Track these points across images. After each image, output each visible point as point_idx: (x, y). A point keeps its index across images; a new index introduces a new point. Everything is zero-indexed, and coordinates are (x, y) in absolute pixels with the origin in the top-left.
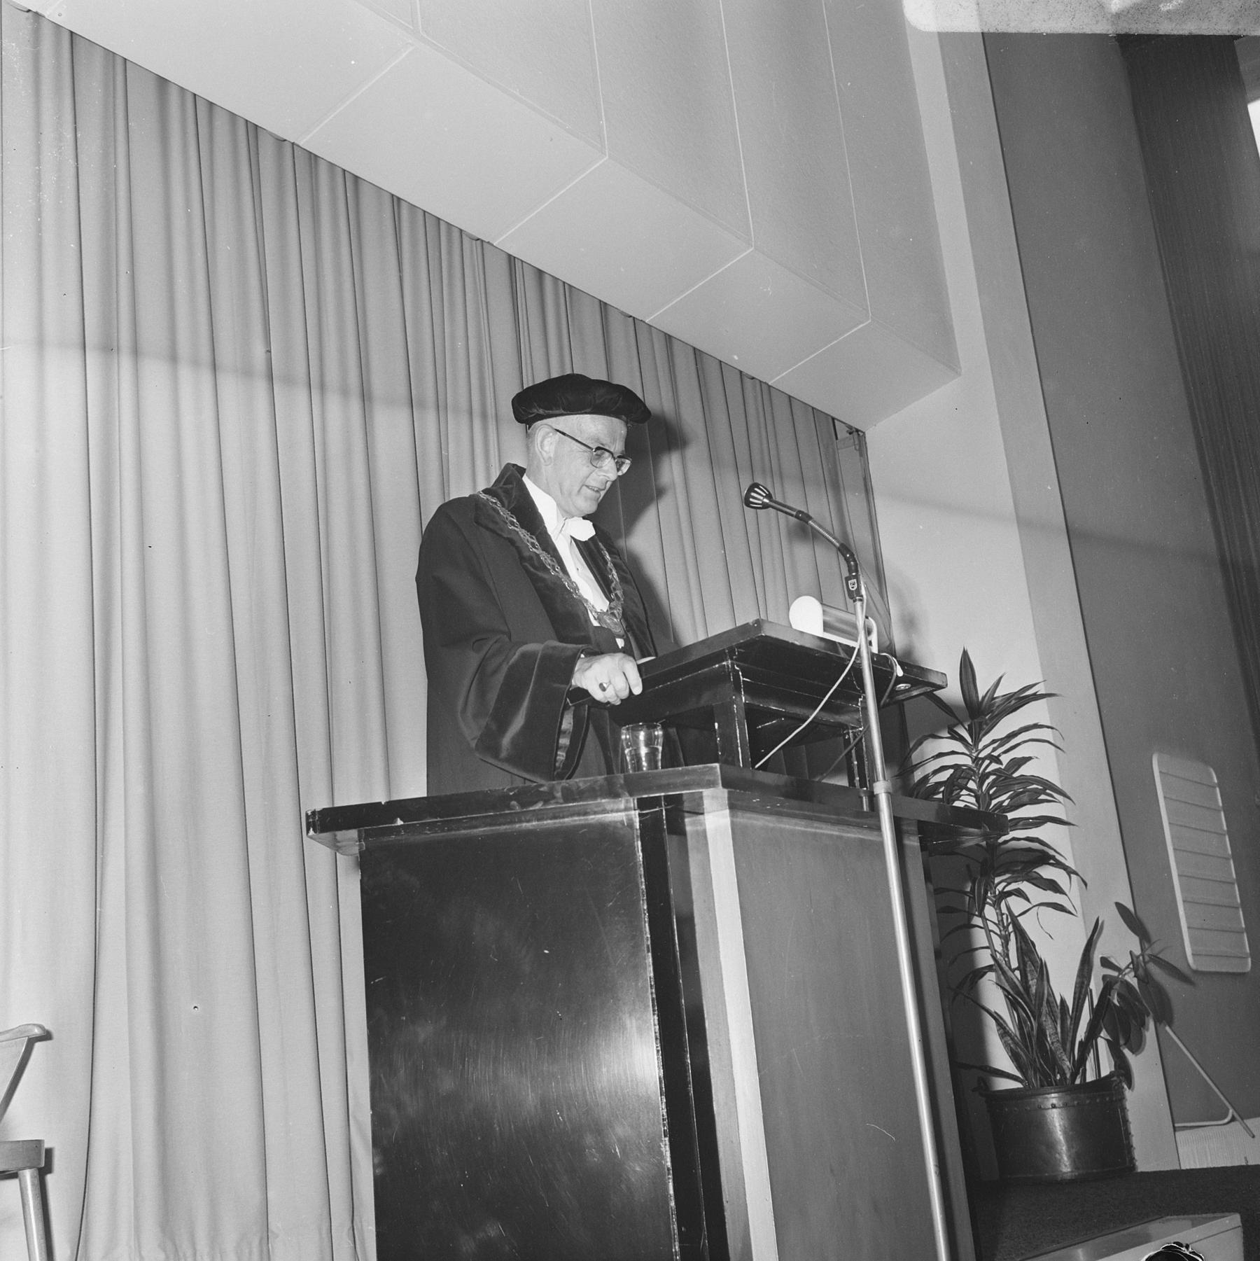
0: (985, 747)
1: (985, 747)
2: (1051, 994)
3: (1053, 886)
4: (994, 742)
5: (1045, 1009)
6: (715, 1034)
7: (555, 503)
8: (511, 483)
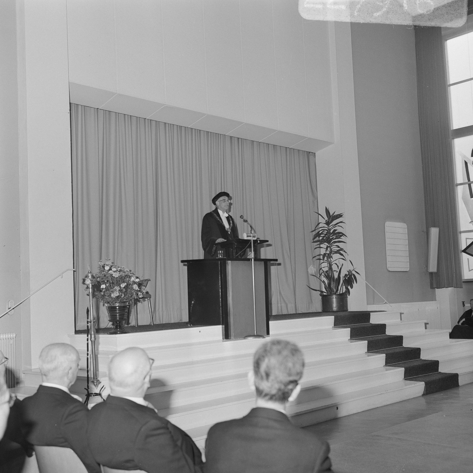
0: (330, 226)
1: (330, 226)
2: (334, 276)
3: (342, 255)
6: (425, 268)
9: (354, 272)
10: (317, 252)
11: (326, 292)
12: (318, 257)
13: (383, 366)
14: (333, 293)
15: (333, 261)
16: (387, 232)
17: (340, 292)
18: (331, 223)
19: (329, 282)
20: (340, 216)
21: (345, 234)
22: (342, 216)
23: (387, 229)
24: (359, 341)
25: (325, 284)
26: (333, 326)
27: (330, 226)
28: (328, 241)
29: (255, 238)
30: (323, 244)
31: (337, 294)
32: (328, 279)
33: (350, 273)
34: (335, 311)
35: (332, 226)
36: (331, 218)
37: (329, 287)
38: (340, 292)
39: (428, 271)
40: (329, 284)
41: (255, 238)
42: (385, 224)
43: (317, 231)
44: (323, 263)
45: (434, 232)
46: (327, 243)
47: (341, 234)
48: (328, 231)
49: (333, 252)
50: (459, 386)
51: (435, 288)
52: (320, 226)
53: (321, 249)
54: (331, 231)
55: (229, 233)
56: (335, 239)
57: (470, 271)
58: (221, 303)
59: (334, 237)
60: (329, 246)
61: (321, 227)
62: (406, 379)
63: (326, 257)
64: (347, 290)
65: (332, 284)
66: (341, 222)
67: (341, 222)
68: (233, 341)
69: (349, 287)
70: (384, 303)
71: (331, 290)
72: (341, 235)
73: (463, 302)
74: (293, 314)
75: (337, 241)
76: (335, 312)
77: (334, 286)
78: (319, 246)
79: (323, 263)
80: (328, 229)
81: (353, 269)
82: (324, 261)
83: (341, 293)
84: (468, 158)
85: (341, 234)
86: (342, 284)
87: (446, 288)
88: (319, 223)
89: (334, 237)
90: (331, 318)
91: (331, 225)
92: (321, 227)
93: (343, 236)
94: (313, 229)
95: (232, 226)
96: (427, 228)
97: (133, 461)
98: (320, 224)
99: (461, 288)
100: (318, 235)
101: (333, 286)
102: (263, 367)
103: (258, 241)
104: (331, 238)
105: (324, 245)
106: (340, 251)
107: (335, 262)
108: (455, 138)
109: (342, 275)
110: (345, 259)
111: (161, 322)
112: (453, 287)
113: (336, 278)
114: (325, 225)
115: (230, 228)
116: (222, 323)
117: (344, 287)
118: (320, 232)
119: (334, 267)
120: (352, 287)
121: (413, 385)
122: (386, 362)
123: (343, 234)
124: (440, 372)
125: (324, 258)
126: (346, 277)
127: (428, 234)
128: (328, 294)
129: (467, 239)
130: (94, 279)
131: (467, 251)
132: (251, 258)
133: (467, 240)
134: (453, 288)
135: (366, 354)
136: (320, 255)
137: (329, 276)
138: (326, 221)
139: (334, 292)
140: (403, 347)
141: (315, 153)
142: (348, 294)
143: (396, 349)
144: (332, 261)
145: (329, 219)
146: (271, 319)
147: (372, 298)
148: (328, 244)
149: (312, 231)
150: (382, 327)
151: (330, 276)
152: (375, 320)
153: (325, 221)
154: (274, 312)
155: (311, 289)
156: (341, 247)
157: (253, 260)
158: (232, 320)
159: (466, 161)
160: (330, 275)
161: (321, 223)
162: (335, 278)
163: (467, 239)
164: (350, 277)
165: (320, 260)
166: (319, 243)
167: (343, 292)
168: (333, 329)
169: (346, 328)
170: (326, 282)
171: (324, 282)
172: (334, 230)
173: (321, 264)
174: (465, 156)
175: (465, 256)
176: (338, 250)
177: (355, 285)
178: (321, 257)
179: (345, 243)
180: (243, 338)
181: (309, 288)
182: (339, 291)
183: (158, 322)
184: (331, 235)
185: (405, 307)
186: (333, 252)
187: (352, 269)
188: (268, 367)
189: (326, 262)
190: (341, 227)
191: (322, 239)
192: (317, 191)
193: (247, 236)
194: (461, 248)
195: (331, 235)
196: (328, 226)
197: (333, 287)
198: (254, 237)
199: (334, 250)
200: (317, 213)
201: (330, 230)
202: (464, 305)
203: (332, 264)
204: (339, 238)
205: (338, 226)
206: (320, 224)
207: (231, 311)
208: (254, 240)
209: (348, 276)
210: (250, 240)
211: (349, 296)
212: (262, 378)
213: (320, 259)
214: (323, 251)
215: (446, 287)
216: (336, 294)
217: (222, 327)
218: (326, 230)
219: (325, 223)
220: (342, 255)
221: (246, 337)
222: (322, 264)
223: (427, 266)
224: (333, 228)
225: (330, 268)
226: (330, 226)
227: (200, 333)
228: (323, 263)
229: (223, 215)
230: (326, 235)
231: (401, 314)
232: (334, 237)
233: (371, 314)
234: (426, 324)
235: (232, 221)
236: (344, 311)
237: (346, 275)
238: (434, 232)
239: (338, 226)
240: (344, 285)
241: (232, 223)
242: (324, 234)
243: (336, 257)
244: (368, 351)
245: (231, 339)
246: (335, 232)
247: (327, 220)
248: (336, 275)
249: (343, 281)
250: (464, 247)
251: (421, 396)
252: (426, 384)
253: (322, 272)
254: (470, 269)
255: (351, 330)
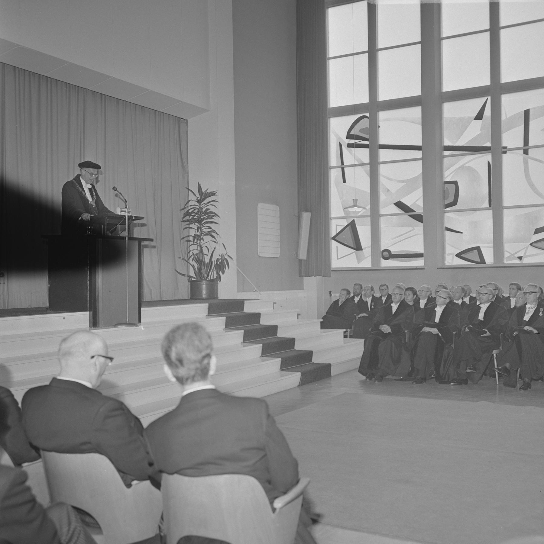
0: (202, 204)
1: (202, 204)
2: (204, 261)
3: (213, 237)
4: (204, 203)
5: (203, 264)
6: (295, 255)
7: (85, 182)
8: (77, 178)
9: (226, 257)
10: (185, 233)
11: (195, 277)
12: (186, 239)
13: (259, 356)
14: (203, 278)
15: (204, 244)
16: (259, 214)
17: (210, 278)
18: (203, 201)
19: (199, 266)
20: (213, 194)
21: (217, 214)
22: (216, 194)
23: (259, 211)
24: (234, 330)
25: (194, 269)
26: (207, 314)
27: (201, 204)
28: (199, 221)
29: (130, 213)
30: (193, 224)
31: (207, 280)
32: (198, 263)
33: (223, 257)
34: (204, 298)
35: (204, 205)
36: (204, 196)
37: (199, 273)
38: (210, 278)
39: (298, 258)
40: (200, 269)
41: (130, 213)
42: (258, 205)
43: (186, 210)
44: (193, 245)
45: (306, 217)
46: (197, 223)
47: (213, 214)
48: (200, 209)
49: (203, 233)
50: (331, 376)
51: (304, 276)
52: (189, 204)
53: (190, 229)
54: (204, 210)
55: (94, 207)
56: (207, 219)
57: (338, 259)
58: (88, 286)
59: (206, 217)
60: (200, 226)
61: (192, 205)
62: (282, 370)
63: (196, 239)
64: (218, 276)
65: (202, 269)
66: (214, 201)
67: (214, 201)
68: (101, 329)
69: (221, 273)
70: (254, 290)
71: (201, 275)
72: (212, 215)
73: (330, 292)
74: (158, 301)
75: (209, 222)
76: (205, 299)
77: (204, 271)
78: (188, 226)
79: (191, 245)
80: (200, 207)
81: (226, 253)
82: (194, 243)
83: (211, 279)
84: (342, 140)
85: (213, 214)
86: (213, 269)
87: (315, 276)
88: (190, 201)
89: (205, 216)
90: (204, 306)
91: (203, 203)
92: (192, 205)
93: (216, 216)
94: (182, 207)
95: (95, 198)
96: (298, 212)
97: (90, 443)
98: (191, 201)
99: (329, 277)
100: (188, 214)
101: (203, 271)
102: (173, 355)
103: (133, 218)
104: (202, 218)
105: (195, 226)
106: (212, 232)
107: (206, 245)
108: (331, 117)
109: (214, 259)
110: (217, 242)
111: (5, 307)
112: (321, 275)
113: (207, 263)
114: (196, 202)
115: (94, 201)
116: (89, 309)
117: (215, 272)
118: (191, 211)
119: (205, 251)
120: (223, 273)
121: (290, 376)
122: (262, 352)
123: (216, 215)
124: (313, 363)
125: (194, 240)
126: (218, 262)
127: (299, 218)
128: (197, 279)
129: (337, 225)
130: (454, 286)
131: (336, 238)
132: (125, 236)
133: (337, 227)
134: (321, 277)
135: (242, 344)
136: (189, 236)
137: (200, 261)
138: (197, 198)
139: (204, 278)
140: (278, 337)
141: (187, 120)
142: (219, 280)
143: (270, 339)
144: (203, 244)
145: (201, 196)
146: (142, 306)
147: (242, 285)
148: (199, 224)
149: (183, 209)
150: (256, 317)
151: (201, 260)
152: (248, 308)
153: (196, 198)
154: (147, 297)
155: (180, 273)
156: (213, 229)
157: (127, 238)
158: (101, 305)
159: (341, 143)
160: (201, 258)
161: (191, 201)
162: (206, 263)
163: (337, 225)
164: (222, 261)
165: (189, 242)
166: (188, 223)
167: (214, 278)
168: (207, 318)
169: (221, 316)
170: (196, 266)
171: (193, 266)
172: (207, 209)
173: (189, 246)
174: (340, 138)
175: (334, 244)
176: (209, 231)
177: (226, 270)
178: (191, 239)
179: (218, 225)
180: (113, 327)
181: (175, 271)
182: (209, 277)
183: (2, 306)
184: (203, 215)
185: (278, 296)
186: (203, 233)
187: (224, 253)
188: (177, 354)
189: (195, 244)
190: (215, 206)
191: (192, 218)
192: (188, 163)
193: (121, 211)
194: (331, 236)
195: (203, 215)
196: (199, 204)
197: (204, 272)
198: (129, 212)
199: (206, 231)
200: (186, 188)
201: (202, 208)
202: (331, 295)
203: (203, 246)
204: (211, 218)
205: (211, 205)
206: (190, 202)
207: (100, 296)
208: (128, 216)
209: (220, 261)
210: (124, 216)
211: (220, 282)
212: (177, 366)
213: (189, 241)
214: (192, 232)
215: (315, 275)
216: (206, 279)
217: (89, 313)
218: (197, 208)
219: (196, 201)
220: (213, 237)
221: (116, 325)
222: (190, 247)
223: (297, 253)
224: (205, 207)
225: (201, 251)
226: (201, 204)
227: (64, 320)
228: (191, 245)
229: (86, 187)
230: (196, 214)
231: (274, 303)
232: (205, 217)
233: (245, 302)
234: (298, 315)
235: (95, 192)
236: (214, 298)
237: (218, 260)
238: (306, 217)
239: (211, 205)
240: (216, 271)
241: (95, 195)
242: (195, 213)
243: (207, 238)
244: (243, 341)
245: (99, 327)
246: (208, 211)
247: (199, 197)
248: (207, 260)
249: (215, 266)
250: (333, 234)
251: (296, 387)
252: (302, 374)
253: (192, 254)
254: (339, 258)
255: (226, 319)
